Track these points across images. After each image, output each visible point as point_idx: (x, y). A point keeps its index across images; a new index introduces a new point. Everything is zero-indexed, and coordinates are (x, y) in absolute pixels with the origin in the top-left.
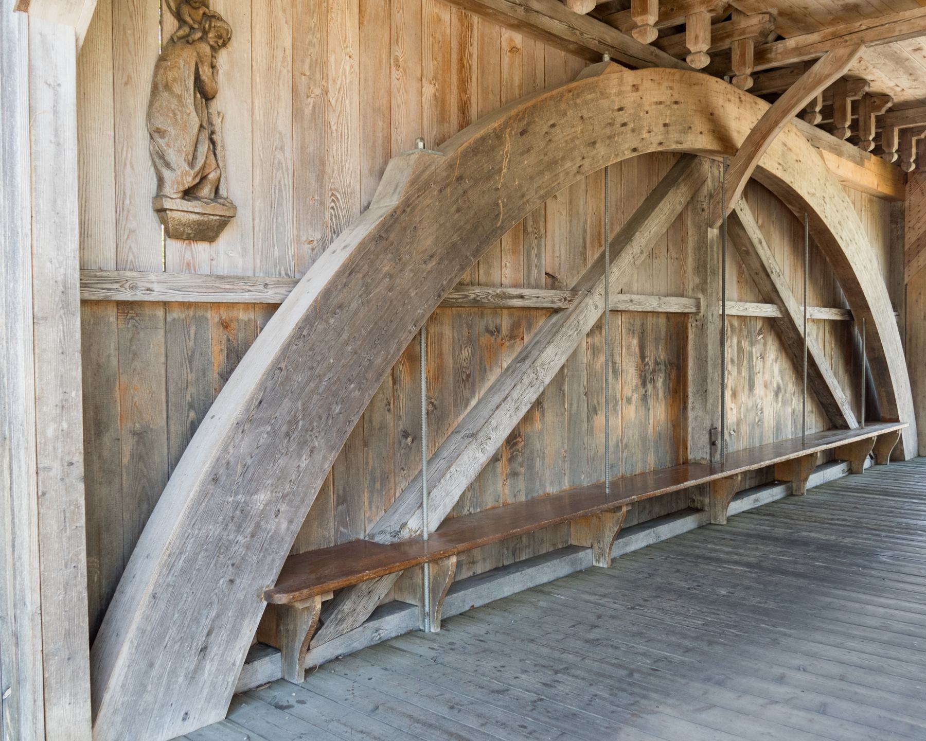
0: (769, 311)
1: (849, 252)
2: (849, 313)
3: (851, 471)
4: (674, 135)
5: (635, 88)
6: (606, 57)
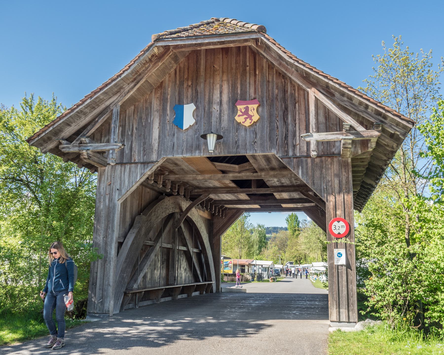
0: (184, 249)
1: (202, 235)
2: (201, 250)
3: (200, 294)
4: (174, 210)
5: (169, 201)
6: (164, 194)
